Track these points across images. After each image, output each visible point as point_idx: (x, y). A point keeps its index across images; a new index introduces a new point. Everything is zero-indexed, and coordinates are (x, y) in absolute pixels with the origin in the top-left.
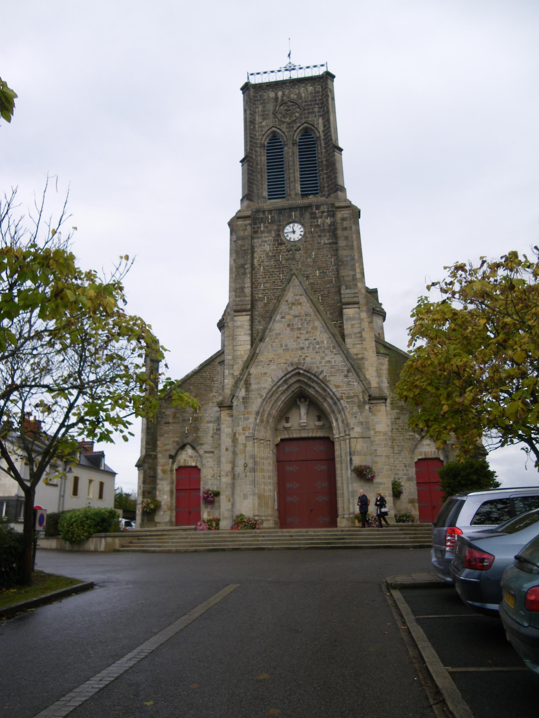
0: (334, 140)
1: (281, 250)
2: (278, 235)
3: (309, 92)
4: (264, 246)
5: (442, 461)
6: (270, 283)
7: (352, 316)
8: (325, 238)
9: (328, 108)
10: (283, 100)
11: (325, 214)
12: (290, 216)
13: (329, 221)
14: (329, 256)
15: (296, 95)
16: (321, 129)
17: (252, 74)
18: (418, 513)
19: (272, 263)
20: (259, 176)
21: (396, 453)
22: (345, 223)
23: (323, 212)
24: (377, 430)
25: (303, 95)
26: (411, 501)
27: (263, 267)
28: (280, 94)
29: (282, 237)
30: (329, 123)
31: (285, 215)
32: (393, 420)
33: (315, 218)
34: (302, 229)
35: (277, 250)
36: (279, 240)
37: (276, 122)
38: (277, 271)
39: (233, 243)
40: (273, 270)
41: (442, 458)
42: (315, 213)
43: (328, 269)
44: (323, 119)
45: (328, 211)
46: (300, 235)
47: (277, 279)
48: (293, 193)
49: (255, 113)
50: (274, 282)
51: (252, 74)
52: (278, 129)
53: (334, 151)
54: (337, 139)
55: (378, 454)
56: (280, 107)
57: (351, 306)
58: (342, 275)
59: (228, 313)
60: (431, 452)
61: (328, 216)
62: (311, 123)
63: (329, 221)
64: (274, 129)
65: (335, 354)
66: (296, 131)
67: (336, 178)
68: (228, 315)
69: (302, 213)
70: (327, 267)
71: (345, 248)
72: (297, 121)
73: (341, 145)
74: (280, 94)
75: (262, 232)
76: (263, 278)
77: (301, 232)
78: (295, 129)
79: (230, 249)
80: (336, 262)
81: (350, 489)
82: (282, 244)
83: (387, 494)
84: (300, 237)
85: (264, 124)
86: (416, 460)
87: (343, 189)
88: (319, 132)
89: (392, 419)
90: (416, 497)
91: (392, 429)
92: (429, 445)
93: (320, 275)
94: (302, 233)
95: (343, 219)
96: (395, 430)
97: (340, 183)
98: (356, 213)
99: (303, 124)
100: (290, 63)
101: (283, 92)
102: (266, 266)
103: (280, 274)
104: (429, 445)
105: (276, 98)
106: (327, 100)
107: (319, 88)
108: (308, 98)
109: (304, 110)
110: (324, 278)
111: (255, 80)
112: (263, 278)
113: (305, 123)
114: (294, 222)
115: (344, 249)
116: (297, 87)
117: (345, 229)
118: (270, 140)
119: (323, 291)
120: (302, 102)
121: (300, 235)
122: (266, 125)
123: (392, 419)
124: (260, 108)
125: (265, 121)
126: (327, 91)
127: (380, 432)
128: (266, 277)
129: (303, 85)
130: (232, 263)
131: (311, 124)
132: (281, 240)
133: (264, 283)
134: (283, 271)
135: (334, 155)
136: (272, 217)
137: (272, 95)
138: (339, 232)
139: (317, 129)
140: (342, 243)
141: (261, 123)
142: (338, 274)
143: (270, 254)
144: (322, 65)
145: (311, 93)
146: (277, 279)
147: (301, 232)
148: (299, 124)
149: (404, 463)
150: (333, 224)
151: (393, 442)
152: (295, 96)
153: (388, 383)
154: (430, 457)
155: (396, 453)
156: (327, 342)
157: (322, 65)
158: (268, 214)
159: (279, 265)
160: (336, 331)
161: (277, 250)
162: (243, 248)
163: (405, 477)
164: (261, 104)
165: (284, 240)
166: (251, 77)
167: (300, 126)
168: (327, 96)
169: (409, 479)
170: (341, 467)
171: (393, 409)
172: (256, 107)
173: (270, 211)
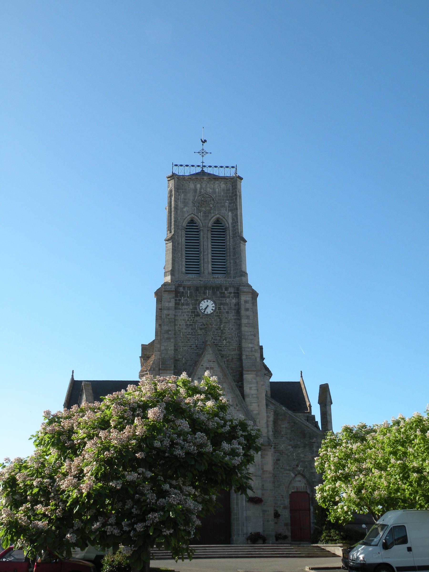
0: (240, 231)
1: (197, 320)
2: (195, 308)
3: (222, 189)
4: (184, 316)
5: (309, 494)
6: (188, 347)
7: (250, 380)
8: (232, 315)
9: (236, 205)
10: (200, 192)
11: (232, 295)
12: (205, 293)
13: (234, 301)
14: (234, 330)
15: (212, 189)
16: (230, 221)
17: (176, 165)
18: (290, 534)
19: (190, 330)
20: (180, 255)
21: (276, 487)
22: (247, 305)
23: (230, 293)
24: (265, 469)
25: (217, 190)
26: (286, 525)
27: (183, 333)
28: (198, 186)
29: (198, 310)
30: (237, 218)
31: (201, 291)
32: (275, 461)
33: (224, 297)
34: (214, 305)
35: (194, 320)
36: (196, 313)
37: (194, 210)
38: (193, 338)
39: (159, 311)
40: (190, 336)
41: (309, 492)
42: (224, 293)
43: (233, 340)
44: (232, 213)
45: (234, 293)
46: (212, 310)
47: (193, 344)
48: (206, 272)
49: (178, 199)
50: (191, 347)
51: (176, 165)
52: (196, 216)
53: (240, 243)
54: (242, 232)
55: (265, 488)
56: (198, 197)
57: (249, 372)
58: (244, 346)
59: (154, 368)
60: (301, 487)
61: (235, 296)
62: (223, 215)
63: (234, 301)
64: (192, 215)
65: (238, 410)
66: (210, 220)
67: (241, 265)
68: (154, 370)
69: (215, 291)
70: (232, 338)
71: (246, 325)
72: (212, 211)
73: (245, 236)
74: (198, 186)
75: (183, 305)
76: (182, 342)
77: (213, 307)
78: (210, 218)
79: (156, 316)
80: (239, 335)
81: (245, 515)
82: (198, 315)
83: (270, 519)
84: (212, 311)
85: (185, 210)
86: (290, 493)
87: (244, 274)
88: (228, 224)
89: (274, 460)
90: (289, 522)
91: (274, 468)
92: (300, 481)
93: (226, 344)
94: (214, 308)
95: (246, 302)
96: (276, 469)
97: (243, 269)
98: (255, 295)
99: (216, 215)
100: (203, 149)
101: (201, 185)
102: (185, 333)
103: (195, 340)
104: (300, 481)
105: (195, 190)
106: (236, 199)
107: (229, 186)
108: (221, 194)
109: (217, 203)
110: (229, 346)
111: (181, 171)
112: (182, 342)
113: (218, 214)
114: (208, 298)
115: (246, 326)
116: (212, 183)
117: (247, 310)
118: (189, 223)
119: (228, 357)
120: (216, 196)
121: (212, 310)
122: (188, 212)
123: (274, 460)
124: (182, 195)
125: (186, 208)
126: (236, 191)
127: (267, 471)
128: (184, 342)
129: (217, 182)
130: (158, 327)
131: (222, 216)
132: (197, 312)
133: (183, 346)
134: (198, 338)
135: (240, 247)
136: (190, 292)
137: (192, 186)
138: (243, 312)
139: (227, 221)
140: (244, 321)
141: (183, 208)
142: (240, 344)
143: (188, 323)
144: (233, 167)
145: (223, 190)
146: (193, 344)
147: (213, 307)
148: (213, 215)
149: (282, 495)
150: (238, 304)
151: (274, 478)
152: (211, 190)
153: (273, 431)
154: (300, 490)
155: (276, 487)
156: (232, 400)
157: (233, 167)
158: (187, 290)
159: (195, 333)
160: (238, 392)
161: (194, 320)
162: (168, 317)
163: (282, 506)
164: (183, 192)
165: (200, 313)
166: (175, 168)
167: (214, 216)
168: (236, 195)
169: (285, 508)
170: (237, 498)
171: (276, 452)
172: (179, 195)
173: (189, 288)
